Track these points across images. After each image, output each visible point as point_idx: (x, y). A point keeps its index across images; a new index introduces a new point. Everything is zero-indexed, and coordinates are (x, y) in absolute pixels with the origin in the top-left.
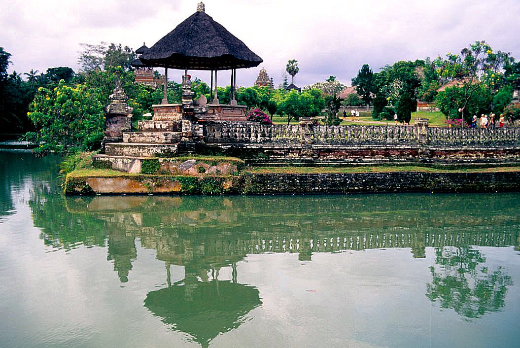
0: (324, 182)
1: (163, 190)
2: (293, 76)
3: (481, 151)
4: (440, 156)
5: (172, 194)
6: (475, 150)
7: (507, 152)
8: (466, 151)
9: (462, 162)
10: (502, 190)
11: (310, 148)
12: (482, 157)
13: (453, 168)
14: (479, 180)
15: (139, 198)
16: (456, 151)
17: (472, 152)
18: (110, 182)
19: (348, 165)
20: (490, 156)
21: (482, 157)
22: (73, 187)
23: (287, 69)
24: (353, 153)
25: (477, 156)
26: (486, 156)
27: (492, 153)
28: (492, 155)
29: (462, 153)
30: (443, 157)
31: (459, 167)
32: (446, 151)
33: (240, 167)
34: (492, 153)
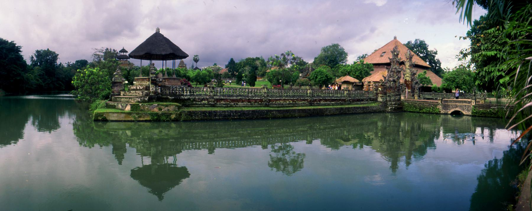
0: (220, 115)
1: (142, 119)
2: (197, 63)
3: (291, 100)
4: (273, 102)
5: (146, 121)
6: (288, 99)
7: (302, 100)
8: (284, 100)
9: (282, 104)
10: (301, 117)
11: (213, 98)
12: (291, 102)
13: (279, 107)
14: (290, 112)
15: (129, 123)
16: (280, 100)
17: (287, 100)
18: (115, 115)
19: (231, 106)
20: (295, 102)
21: (291, 102)
22: (98, 117)
23: (193, 60)
24: (233, 101)
25: (289, 102)
26: (293, 102)
27: (295, 100)
28: (296, 101)
29: (282, 101)
30: (274, 102)
31: (281, 107)
32: (275, 99)
33: (179, 108)
34: (295, 100)
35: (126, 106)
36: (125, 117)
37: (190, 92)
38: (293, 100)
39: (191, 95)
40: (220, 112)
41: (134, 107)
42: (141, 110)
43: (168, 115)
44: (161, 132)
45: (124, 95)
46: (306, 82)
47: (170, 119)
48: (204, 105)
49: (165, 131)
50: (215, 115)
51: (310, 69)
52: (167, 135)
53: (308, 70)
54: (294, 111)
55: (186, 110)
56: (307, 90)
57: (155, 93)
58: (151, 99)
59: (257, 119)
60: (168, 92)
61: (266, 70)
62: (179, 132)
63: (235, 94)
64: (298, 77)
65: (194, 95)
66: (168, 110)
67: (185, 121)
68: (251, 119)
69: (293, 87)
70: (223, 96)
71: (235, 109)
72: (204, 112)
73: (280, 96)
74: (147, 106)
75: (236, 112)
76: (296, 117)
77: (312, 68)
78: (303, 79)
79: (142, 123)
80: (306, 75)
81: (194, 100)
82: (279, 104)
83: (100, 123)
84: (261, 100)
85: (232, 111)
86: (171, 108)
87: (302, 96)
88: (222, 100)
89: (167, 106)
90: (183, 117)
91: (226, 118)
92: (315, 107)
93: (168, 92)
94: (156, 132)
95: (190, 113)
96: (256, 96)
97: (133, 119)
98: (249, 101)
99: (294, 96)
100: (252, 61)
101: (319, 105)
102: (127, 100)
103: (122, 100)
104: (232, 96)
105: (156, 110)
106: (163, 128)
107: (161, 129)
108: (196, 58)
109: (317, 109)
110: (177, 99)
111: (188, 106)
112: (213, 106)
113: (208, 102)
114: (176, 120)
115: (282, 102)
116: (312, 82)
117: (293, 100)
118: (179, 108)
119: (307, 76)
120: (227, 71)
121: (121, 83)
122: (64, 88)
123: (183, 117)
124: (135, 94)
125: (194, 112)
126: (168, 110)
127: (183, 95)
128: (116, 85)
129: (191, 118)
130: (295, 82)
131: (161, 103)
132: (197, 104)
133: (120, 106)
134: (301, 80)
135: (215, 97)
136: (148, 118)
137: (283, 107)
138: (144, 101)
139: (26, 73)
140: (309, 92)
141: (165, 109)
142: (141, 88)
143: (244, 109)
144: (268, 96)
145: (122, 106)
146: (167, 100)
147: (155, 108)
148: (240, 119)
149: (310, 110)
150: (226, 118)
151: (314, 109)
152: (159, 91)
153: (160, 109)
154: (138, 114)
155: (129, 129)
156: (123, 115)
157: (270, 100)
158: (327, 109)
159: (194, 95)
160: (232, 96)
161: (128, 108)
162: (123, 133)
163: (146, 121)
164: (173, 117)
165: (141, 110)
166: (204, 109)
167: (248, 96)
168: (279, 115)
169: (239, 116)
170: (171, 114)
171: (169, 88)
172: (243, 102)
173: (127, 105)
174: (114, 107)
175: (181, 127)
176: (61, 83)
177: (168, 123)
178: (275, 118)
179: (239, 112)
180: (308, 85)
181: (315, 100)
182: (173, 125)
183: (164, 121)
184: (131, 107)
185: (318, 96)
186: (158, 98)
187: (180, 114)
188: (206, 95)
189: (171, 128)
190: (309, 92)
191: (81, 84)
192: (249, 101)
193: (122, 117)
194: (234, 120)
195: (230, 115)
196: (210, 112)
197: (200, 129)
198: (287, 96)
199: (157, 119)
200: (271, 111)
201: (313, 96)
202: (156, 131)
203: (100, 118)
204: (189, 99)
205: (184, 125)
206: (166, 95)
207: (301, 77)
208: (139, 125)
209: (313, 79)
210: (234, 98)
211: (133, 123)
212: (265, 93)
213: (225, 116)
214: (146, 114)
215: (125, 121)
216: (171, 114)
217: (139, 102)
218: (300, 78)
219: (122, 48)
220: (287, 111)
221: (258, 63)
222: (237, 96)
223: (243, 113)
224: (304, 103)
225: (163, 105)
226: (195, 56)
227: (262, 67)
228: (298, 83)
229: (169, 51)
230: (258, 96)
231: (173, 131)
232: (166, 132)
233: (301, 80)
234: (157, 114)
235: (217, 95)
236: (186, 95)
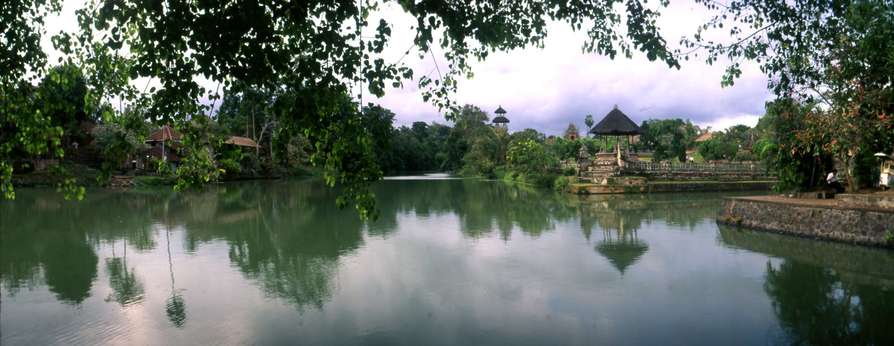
1: (617, 192)
5: (621, 193)
8: (730, 174)
11: (671, 172)
12: (736, 177)
13: (726, 181)
15: (607, 195)
18: (596, 188)
19: (686, 180)
21: (736, 177)
24: (687, 175)
35: (602, 181)
36: (604, 190)
37: (652, 167)
38: (738, 175)
39: (652, 170)
40: (679, 185)
41: (610, 181)
42: (616, 184)
43: (638, 187)
44: (632, 203)
45: (593, 170)
46: (748, 156)
47: (640, 190)
48: (664, 179)
49: (635, 203)
50: (676, 188)
51: (752, 137)
52: (637, 206)
53: (750, 139)
54: (739, 184)
55: (653, 183)
56: (750, 164)
57: (624, 167)
58: (622, 174)
59: (709, 191)
60: (634, 167)
61: (695, 139)
62: (647, 203)
63: (688, 169)
64: (737, 149)
65: (654, 170)
66: (637, 183)
67: (652, 193)
68: (704, 191)
69: (732, 162)
70: (680, 170)
71: (690, 182)
72: (667, 185)
73: (726, 171)
74: (619, 180)
75: (691, 184)
76: (741, 190)
77: (754, 135)
78: (744, 152)
79: (617, 195)
80: (748, 146)
81: (656, 174)
82: (726, 178)
83: (583, 196)
84: (710, 175)
85: (688, 184)
86: (639, 181)
87: (746, 171)
88: (678, 174)
89: (636, 180)
90: (650, 189)
91: (685, 190)
92: (758, 182)
93: (634, 167)
94: (627, 204)
95: (656, 186)
96: (705, 170)
97: (610, 192)
98: (700, 175)
99: (738, 171)
100: (672, 124)
101: (762, 179)
102: (600, 174)
103: (594, 175)
104: (686, 171)
105: (627, 183)
106: (634, 199)
107: (632, 200)
108: (590, 120)
109: (760, 183)
110: (642, 174)
111: (651, 180)
112: (672, 180)
113: (668, 176)
114: (644, 192)
115: (728, 176)
116: (755, 156)
117: (738, 175)
118: (646, 181)
119: (749, 147)
120: (639, 140)
121: (587, 158)
122: (403, 166)
123: (650, 189)
124: (605, 170)
125: (658, 185)
126: (637, 183)
127: (646, 170)
128: (583, 160)
129: (656, 190)
130: (735, 155)
131: (631, 177)
132: (658, 178)
133: (595, 181)
134: (742, 152)
135: (673, 172)
136: (622, 191)
137: (730, 181)
138: (616, 176)
139: (783, 159)
140: (752, 166)
141: (634, 183)
142: (609, 163)
143: (697, 182)
144: (716, 170)
145: (598, 181)
146: (634, 174)
147: (626, 181)
148: (695, 191)
149: (753, 183)
150: (685, 190)
151: (757, 183)
152: (627, 166)
153: (631, 183)
154: (614, 187)
155: (607, 200)
156: (602, 188)
157: (718, 175)
158: (769, 183)
159: (654, 170)
160: (686, 171)
161: (605, 182)
162: (599, 205)
163: (621, 193)
164: (642, 189)
165: (616, 184)
166: (665, 183)
167: (699, 171)
168: (726, 188)
169: (694, 188)
170: (640, 187)
171: (634, 163)
172: (695, 176)
173: (603, 179)
174: (589, 182)
175: (648, 199)
176: (399, 158)
177: (638, 195)
178: (723, 190)
179: (694, 184)
180: (750, 159)
181: (758, 175)
182: (642, 197)
183: (635, 193)
184: (608, 181)
185: (760, 171)
186: (626, 172)
187: (648, 187)
188: (665, 170)
189: (640, 199)
190: (752, 166)
191: (272, 164)
192: (700, 175)
193: (601, 190)
194: (691, 192)
195: (687, 188)
196: (671, 185)
197: (664, 202)
198: (732, 171)
199: (629, 191)
200: (720, 184)
201: (756, 171)
202: (628, 203)
203: (583, 192)
204: (651, 174)
205: (650, 196)
206: (632, 169)
207: (741, 148)
208: (616, 197)
209: (756, 152)
210: (688, 172)
211: (610, 195)
212: (713, 167)
213: (683, 188)
214: (620, 187)
215: (604, 194)
216: (640, 187)
217: (612, 176)
218: (740, 150)
219: (498, 107)
220: (734, 184)
221: (683, 129)
222: (690, 171)
223: (697, 186)
224: (748, 178)
225: (633, 179)
226: (587, 116)
227: (689, 134)
228: (739, 158)
229: (632, 129)
230: (707, 171)
231: (639, 203)
232: (636, 203)
233: (742, 152)
234: (629, 187)
235: (673, 170)
236: (649, 170)
